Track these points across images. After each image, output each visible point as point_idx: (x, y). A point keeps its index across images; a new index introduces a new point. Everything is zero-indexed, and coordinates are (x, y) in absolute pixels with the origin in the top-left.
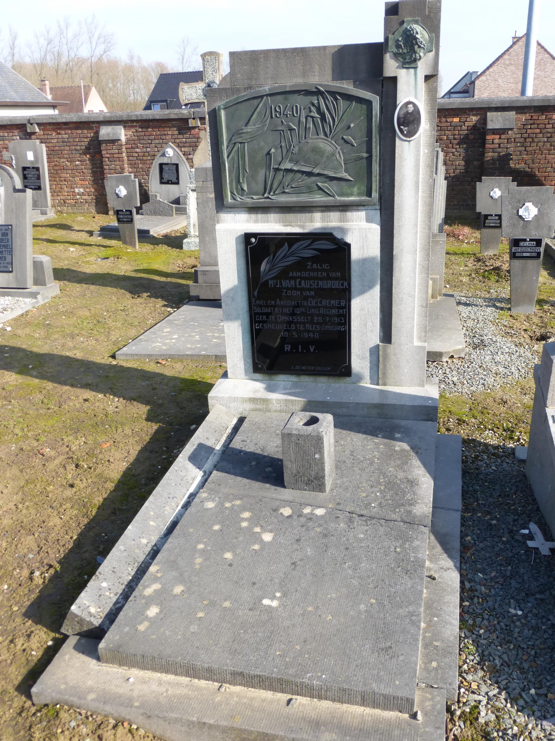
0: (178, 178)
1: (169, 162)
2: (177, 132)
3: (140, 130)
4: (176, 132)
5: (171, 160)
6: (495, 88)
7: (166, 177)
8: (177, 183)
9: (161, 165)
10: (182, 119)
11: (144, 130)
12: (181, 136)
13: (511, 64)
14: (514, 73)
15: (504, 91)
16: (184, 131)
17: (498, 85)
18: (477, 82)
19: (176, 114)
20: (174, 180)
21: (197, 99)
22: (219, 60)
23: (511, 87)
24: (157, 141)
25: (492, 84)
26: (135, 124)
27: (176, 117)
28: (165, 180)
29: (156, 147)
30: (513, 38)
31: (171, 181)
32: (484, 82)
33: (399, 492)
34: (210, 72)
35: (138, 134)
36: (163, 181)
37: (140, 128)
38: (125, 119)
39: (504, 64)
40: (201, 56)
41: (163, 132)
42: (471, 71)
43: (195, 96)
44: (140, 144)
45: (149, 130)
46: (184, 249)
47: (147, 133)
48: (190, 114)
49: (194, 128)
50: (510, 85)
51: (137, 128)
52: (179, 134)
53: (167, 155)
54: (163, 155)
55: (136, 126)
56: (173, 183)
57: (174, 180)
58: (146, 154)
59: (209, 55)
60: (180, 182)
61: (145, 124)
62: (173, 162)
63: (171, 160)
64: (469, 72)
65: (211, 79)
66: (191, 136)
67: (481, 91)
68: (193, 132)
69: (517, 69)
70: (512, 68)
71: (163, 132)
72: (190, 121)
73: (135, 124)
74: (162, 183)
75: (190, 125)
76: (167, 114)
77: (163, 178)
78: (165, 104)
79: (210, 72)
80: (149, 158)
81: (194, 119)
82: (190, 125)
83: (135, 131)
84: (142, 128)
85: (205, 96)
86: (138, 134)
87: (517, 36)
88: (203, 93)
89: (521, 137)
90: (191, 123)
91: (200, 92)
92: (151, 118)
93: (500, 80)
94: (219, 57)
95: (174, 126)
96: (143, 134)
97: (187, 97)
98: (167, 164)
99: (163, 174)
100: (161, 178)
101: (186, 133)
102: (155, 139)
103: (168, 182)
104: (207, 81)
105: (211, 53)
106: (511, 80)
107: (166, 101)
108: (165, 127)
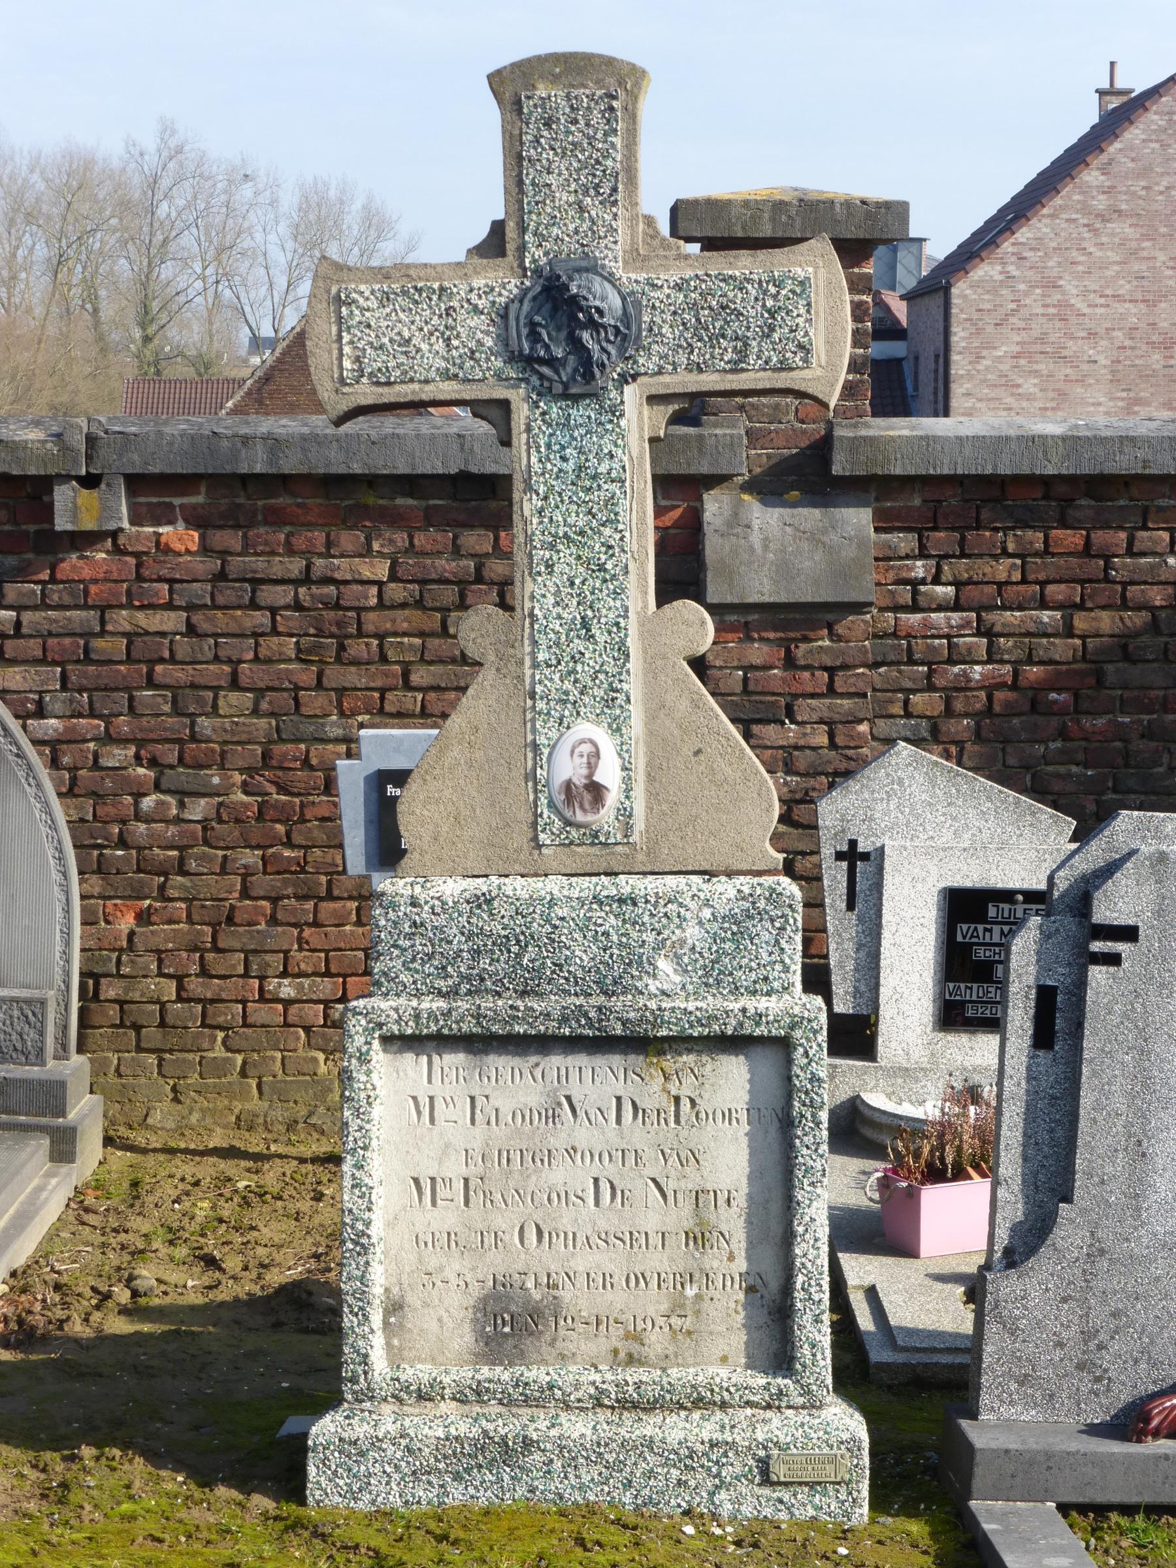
6: (1050, 318)
13: (1119, 212)
14: (1134, 252)
15: (1092, 335)
17: (1058, 305)
18: (961, 290)
21: (447, 376)
22: (632, 118)
23: (1123, 317)
25: (1034, 303)
30: (1101, 93)
32: (994, 291)
34: (563, 197)
39: (1085, 209)
40: (497, 81)
43: (431, 356)
46: (313, 1494)
48: (66, 448)
49: (82, 540)
50: (1121, 308)
59: (555, 79)
65: (570, 246)
66: (56, 594)
67: (979, 331)
68: (72, 564)
69: (1145, 237)
70: (1123, 228)
72: (62, 495)
75: (62, 523)
79: (563, 197)
81: (90, 481)
82: (62, 523)
85: (514, 357)
87: (1120, 84)
88: (503, 340)
90: (71, 508)
91: (477, 330)
93: (1070, 286)
94: (634, 97)
97: (374, 362)
104: (536, 254)
105: (572, 67)
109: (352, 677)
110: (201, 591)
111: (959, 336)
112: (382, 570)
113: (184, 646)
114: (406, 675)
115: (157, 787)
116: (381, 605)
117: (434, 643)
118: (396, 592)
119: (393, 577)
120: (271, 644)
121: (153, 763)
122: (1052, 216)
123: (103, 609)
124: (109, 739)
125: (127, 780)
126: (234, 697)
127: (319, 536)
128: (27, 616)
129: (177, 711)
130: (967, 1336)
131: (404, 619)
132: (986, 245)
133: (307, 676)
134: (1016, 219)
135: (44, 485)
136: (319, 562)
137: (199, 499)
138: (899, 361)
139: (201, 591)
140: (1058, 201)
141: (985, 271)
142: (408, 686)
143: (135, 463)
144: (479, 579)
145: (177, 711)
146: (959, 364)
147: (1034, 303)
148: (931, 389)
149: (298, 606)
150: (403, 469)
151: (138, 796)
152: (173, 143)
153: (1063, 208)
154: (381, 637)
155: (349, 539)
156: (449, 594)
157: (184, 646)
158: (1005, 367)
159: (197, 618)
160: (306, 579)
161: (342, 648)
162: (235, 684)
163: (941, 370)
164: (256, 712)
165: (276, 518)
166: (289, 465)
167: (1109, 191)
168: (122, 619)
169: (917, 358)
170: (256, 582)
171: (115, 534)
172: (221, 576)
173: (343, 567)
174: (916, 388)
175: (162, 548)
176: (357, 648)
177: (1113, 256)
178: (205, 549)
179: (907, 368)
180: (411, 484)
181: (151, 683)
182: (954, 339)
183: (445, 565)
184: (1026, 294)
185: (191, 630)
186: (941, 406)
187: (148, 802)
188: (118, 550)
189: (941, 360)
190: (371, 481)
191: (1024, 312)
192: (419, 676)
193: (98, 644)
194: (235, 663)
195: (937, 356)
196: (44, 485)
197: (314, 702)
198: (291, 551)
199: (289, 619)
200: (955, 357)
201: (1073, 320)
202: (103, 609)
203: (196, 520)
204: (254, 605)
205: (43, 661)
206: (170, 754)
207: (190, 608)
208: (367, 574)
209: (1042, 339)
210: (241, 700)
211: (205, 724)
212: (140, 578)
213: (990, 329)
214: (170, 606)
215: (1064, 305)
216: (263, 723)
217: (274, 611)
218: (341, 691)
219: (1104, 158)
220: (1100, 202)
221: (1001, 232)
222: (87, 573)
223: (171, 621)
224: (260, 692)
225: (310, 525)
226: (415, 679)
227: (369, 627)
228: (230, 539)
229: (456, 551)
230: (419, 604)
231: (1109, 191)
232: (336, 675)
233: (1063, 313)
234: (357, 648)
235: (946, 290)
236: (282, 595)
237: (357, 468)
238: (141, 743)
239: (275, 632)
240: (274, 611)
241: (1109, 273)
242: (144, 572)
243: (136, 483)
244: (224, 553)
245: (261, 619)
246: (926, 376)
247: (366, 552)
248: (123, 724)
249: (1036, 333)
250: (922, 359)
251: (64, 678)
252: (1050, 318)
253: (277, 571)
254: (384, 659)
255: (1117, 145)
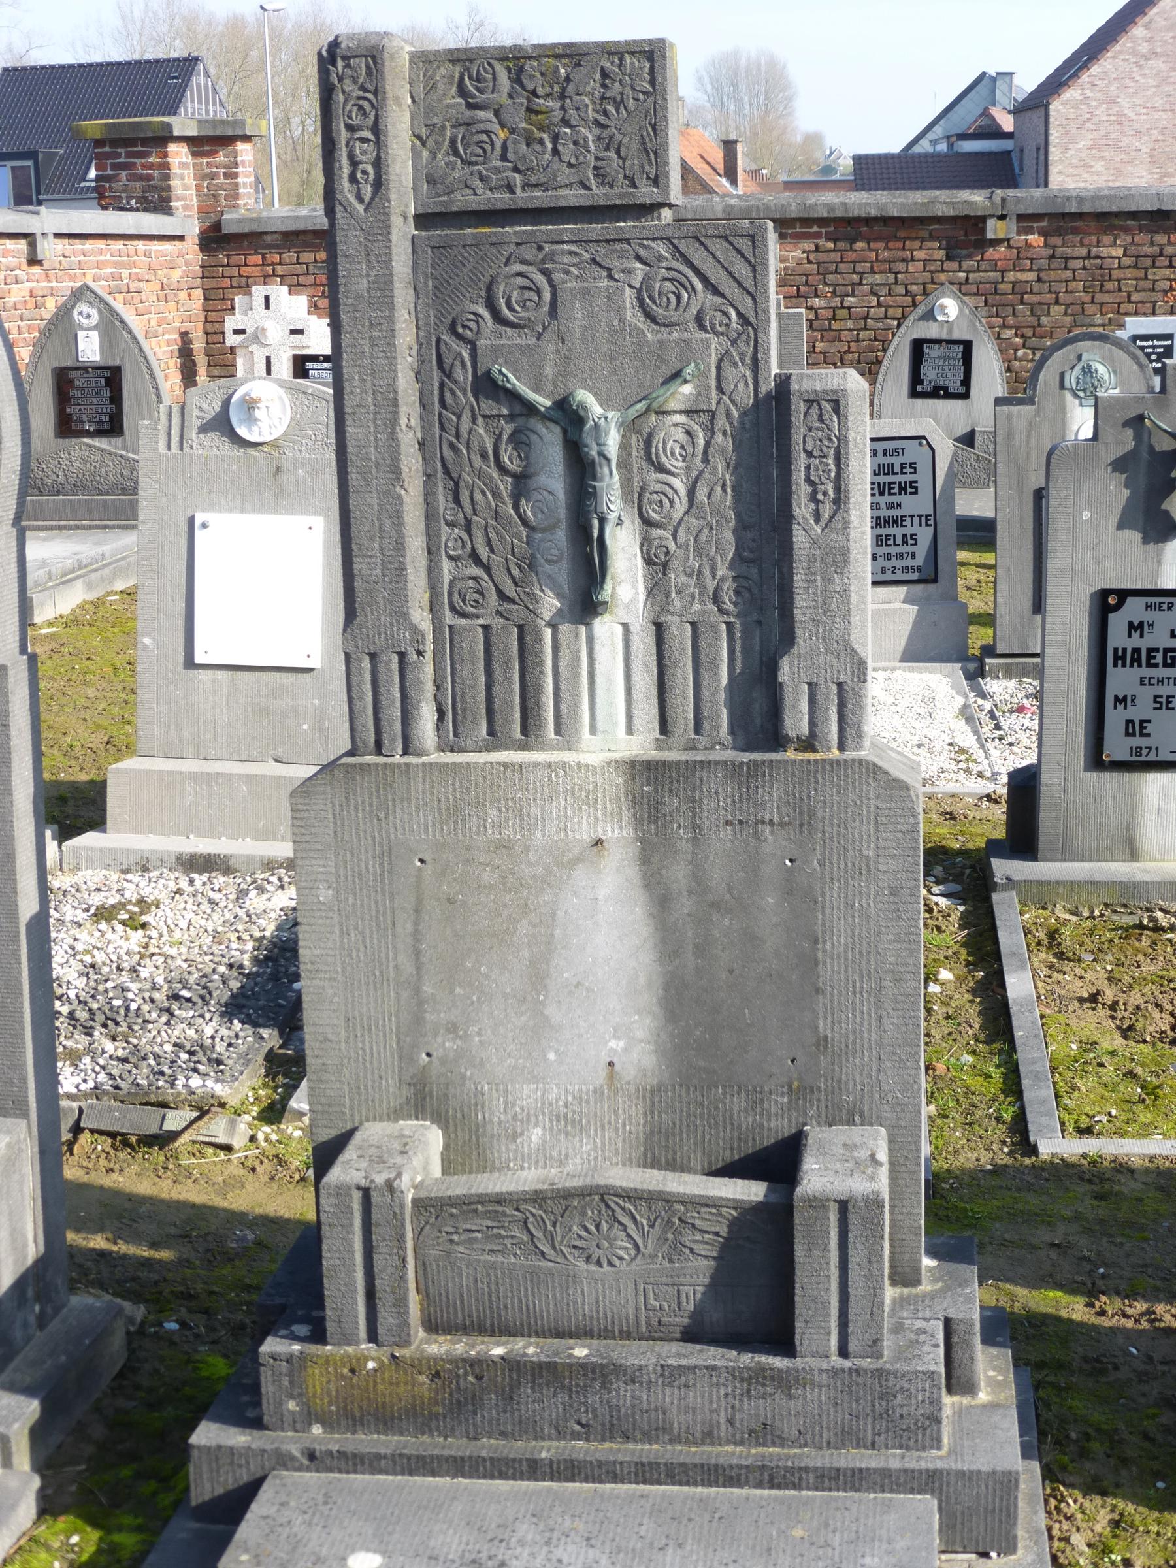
0: (966, 381)
1: (944, 336)
2: (942, 253)
3: (830, 245)
4: (941, 255)
5: (950, 331)
6: (1112, 123)
7: (930, 376)
8: (965, 396)
9: (918, 346)
10: (967, 217)
11: (840, 245)
12: (955, 265)
13: (1155, 53)
16: (964, 252)
19: (952, 203)
20: (956, 386)
23: (1157, 121)
24: (878, 278)
25: (1101, 113)
26: (815, 229)
27: (952, 213)
28: (927, 387)
29: (873, 293)
31: (945, 389)
32: (1076, 107)
33: (1032, 1471)
35: (823, 257)
36: (919, 389)
37: (828, 239)
38: (793, 215)
39: (1134, 52)
41: (900, 254)
42: (992, 72)
44: (826, 284)
45: (859, 245)
47: (850, 256)
48: (993, 204)
50: (1156, 115)
51: (821, 242)
52: (949, 258)
53: (940, 318)
54: (929, 316)
55: (817, 235)
56: (949, 396)
57: (956, 386)
58: (843, 313)
60: (973, 392)
61: (847, 228)
62: (956, 336)
63: (950, 331)
64: (984, 74)
66: (983, 266)
67: (1067, 133)
68: (990, 253)
70: (1158, 64)
71: (900, 254)
72: (991, 223)
73: (815, 229)
74: (914, 394)
75: (990, 235)
76: (923, 204)
77: (921, 382)
78: (29, 163)
80: (850, 324)
81: (1002, 217)
82: (990, 235)
83: (812, 247)
84: (835, 241)
86: (823, 257)
89: (1119, 281)
90: (994, 230)
92: (874, 213)
93: (1124, 102)
95: (932, 238)
96: (836, 256)
98: (938, 342)
99: (924, 369)
100: (916, 379)
101: (970, 257)
102: (873, 272)
103: (937, 393)
106: (1159, 102)
107: (32, 155)
108: (909, 238)
109: (1106, 298)
110: (1044, 263)
111: (1055, 136)
112: (1120, 252)
113: (1036, 287)
114: (1129, 296)
115: (1024, 346)
116: (1119, 267)
117: (1141, 283)
118: (1126, 261)
119: (1125, 255)
120: (1072, 285)
121: (1022, 336)
122: (1114, 57)
123: (1002, 272)
124: (1004, 326)
125: (1012, 344)
126: (1057, 307)
127: (1094, 238)
128: (971, 276)
129: (1032, 314)
130: (769, 1189)
131: (1129, 273)
132: (1071, 77)
133: (1087, 298)
134: (1090, 60)
135: (983, 219)
136: (1094, 250)
137: (1044, 224)
138: (1009, 152)
139: (1044, 263)
140: (1117, 47)
141: (1070, 94)
142: (1129, 302)
143: (1022, 209)
144: (1161, 255)
145: (1032, 314)
146: (1054, 153)
147: (1101, 113)
148: (1033, 170)
149: (1084, 268)
150: (1133, 209)
151: (1016, 350)
152: (477, 19)
153: (1120, 52)
154: (1119, 281)
155: (1107, 239)
156: (1148, 262)
157: (1036, 287)
158: (1083, 155)
159: (1042, 275)
160: (1089, 257)
161: (1102, 286)
162: (1057, 302)
163: (1042, 157)
164: (1066, 314)
165: (1075, 231)
166: (1086, 208)
167: (1149, 40)
168: (1011, 276)
169: (1022, 150)
170: (1067, 259)
171: (1008, 240)
172: (1053, 256)
173: (1103, 251)
174: (1021, 169)
175: (1028, 245)
176: (1109, 286)
177: (1152, 82)
178: (1046, 245)
179: (1015, 157)
180: (1134, 215)
181: (1022, 303)
182: (1051, 138)
183: (1148, 250)
184: (1097, 108)
185: (1039, 280)
186: (1042, 181)
187: (1020, 353)
188: (1010, 247)
189: (1042, 152)
190: (1117, 215)
191: (1096, 120)
192: (1135, 297)
193: (1000, 286)
194: (1057, 293)
195: (1038, 149)
196: (983, 219)
197: (1090, 309)
198: (1082, 245)
199: (1080, 274)
200: (1052, 149)
201: (1126, 123)
202: (1002, 272)
203: (1043, 233)
204: (1066, 268)
205: (977, 294)
206: (1029, 332)
207: (1039, 270)
208: (1114, 254)
209: (1106, 137)
210: (1057, 310)
211: (1044, 320)
212: (1018, 258)
213: (1074, 131)
214: (1031, 270)
215: (1120, 114)
216: (1068, 319)
217: (1074, 271)
218: (1102, 304)
219: (1146, 19)
220: (1144, 48)
221: (1080, 69)
222: (997, 257)
223: (1032, 276)
224: (1067, 306)
225: (1091, 234)
226: (1133, 298)
227: (1114, 277)
228: (1056, 240)
229: (1152, 243)
230: (1136, 266)
231: (1149, 40)
232: (1100, 298)
233: (1120, 120)
234: (1109, 286)
235: (1046, 107)
236: (1078, 264)
237: (1115, 209)
238: (1017, 328)
239: (1074, 279)
240: (1074, 271)
241: (1149, 93)
242: (1021, 254)
243: (1021, 217)
244: (1054, 247)
245: (1069, 274)
246: (1029, 161)
247: (1114, 244)
248: (1010, 320)
249: (1102, 133)
250: (1026, 151)
251: (986, 301)
252: (1112, 123)
253: (1076, 254)
254: (1120, 290)
255: (1155, 10)
